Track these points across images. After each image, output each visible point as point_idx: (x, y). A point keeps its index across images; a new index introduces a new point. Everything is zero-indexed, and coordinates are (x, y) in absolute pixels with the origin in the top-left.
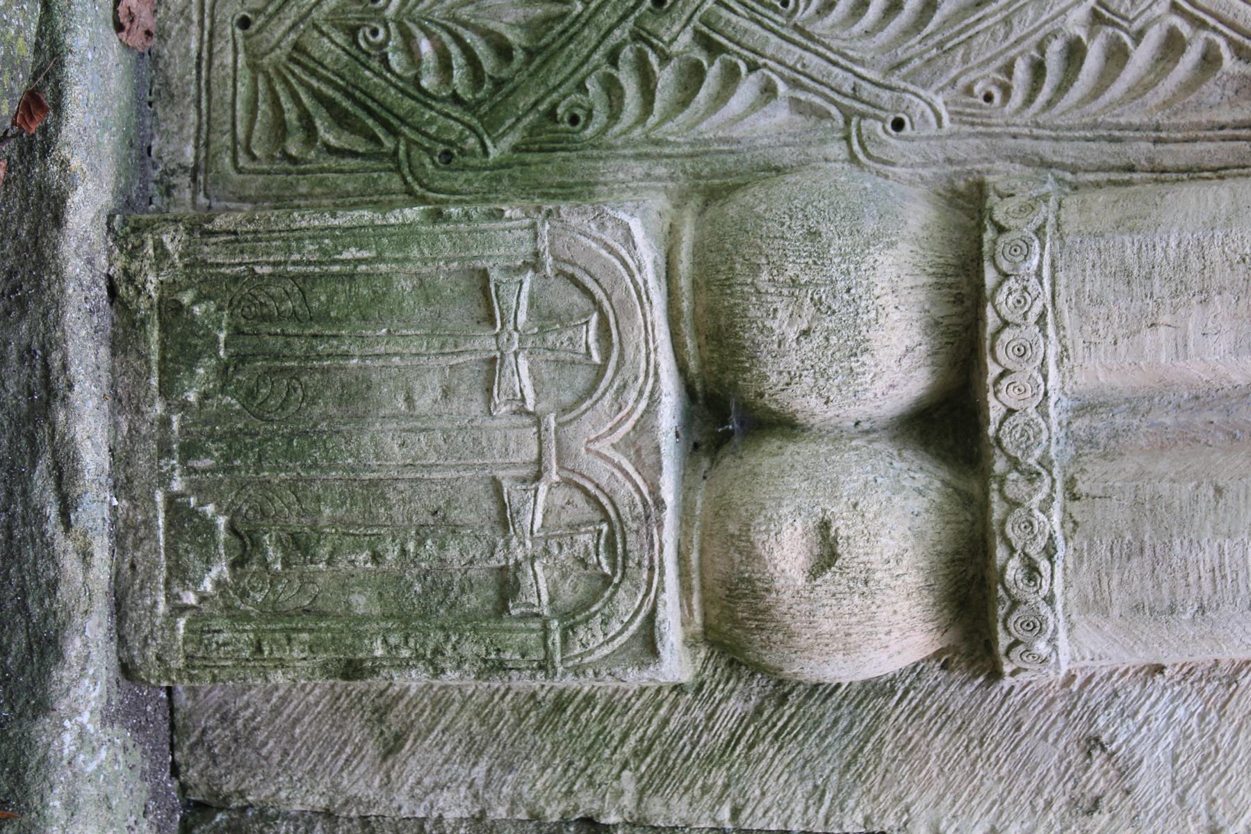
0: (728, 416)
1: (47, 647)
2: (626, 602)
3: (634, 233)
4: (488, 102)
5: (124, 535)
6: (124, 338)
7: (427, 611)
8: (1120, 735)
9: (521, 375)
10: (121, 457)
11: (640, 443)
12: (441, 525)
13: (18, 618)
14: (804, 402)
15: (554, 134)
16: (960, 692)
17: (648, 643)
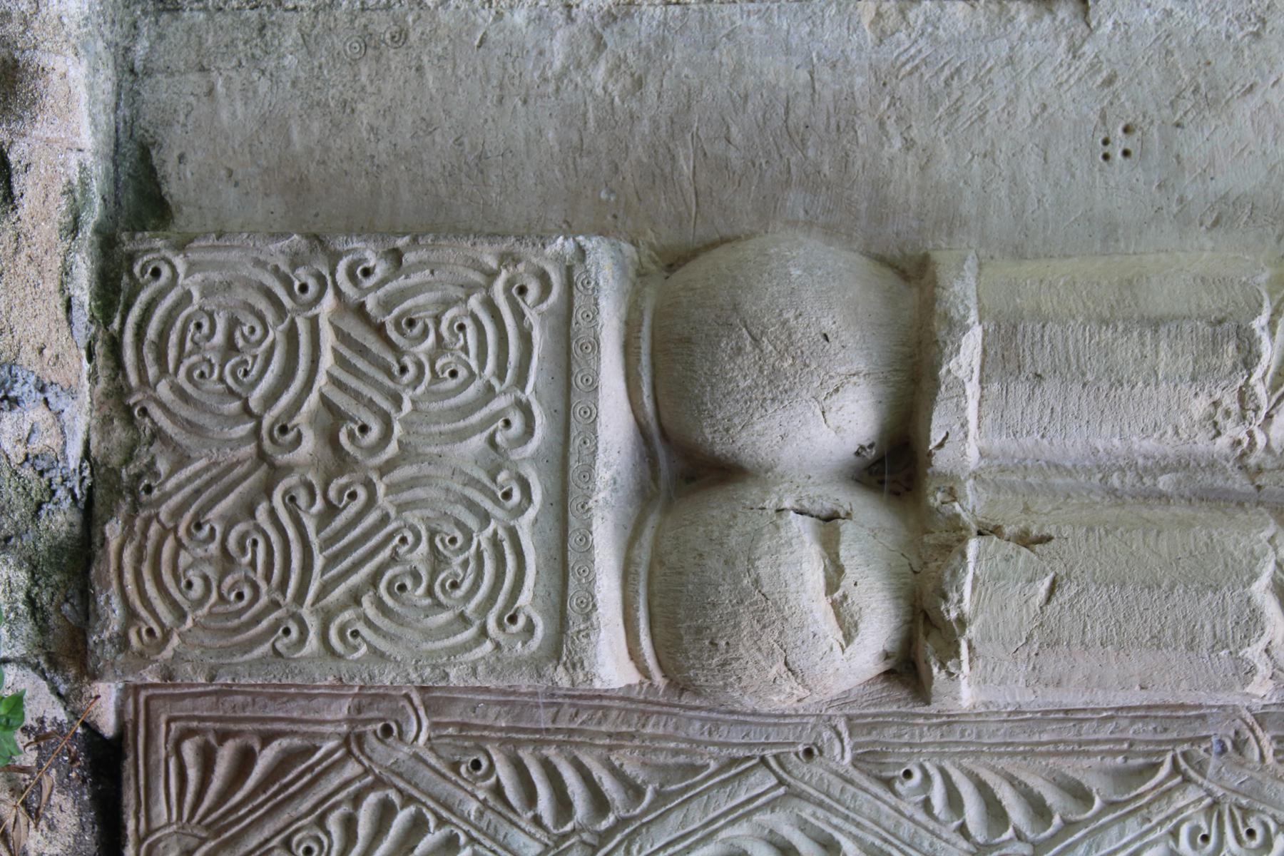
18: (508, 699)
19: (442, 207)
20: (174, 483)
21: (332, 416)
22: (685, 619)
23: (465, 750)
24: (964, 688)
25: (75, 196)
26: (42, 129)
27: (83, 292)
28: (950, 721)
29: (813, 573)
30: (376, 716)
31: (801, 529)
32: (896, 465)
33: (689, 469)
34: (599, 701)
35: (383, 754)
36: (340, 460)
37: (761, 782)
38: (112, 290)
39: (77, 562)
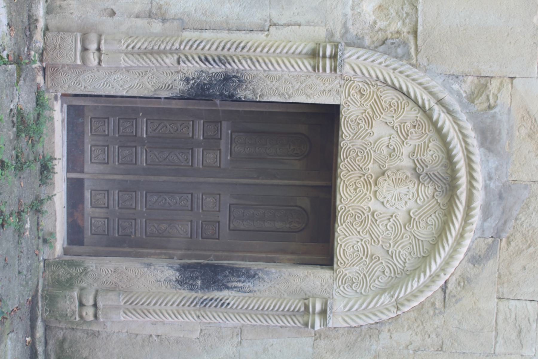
0: (81, 305)
1: (37, 318)
2: (74, 316)
3: (75, 294)
4: (67, 282)
5: (42, 310)
6: (42, 298)
7: (61, 316)
8: (106, 324)
9: (68, 302)
10: (42, 305)
11: (75, 307)
12: (63, 311)
13: (12, 219)
14: (86, 304)
15: (71, 284)
16: (96, 321)
17: (75, 319)
18: (73, 65)
19: (68, 31)
20: (49, 49)
21: (60, 45)
22: (84, 59)
23: (70, 69)
24: (103, 65)
25: (42, 28)
26: (39, 24)
27: (42, 35)
28: (103, 67)
29: (92, 56)
30: (63, 66)
31: (92, 54)
32: (99, 49)
33: (85, 49)
34: (79, 65)
35: (64, 69)
36: (60, 48)
37: (90, 72)
38: (44, 35)
39: (42, 54)
